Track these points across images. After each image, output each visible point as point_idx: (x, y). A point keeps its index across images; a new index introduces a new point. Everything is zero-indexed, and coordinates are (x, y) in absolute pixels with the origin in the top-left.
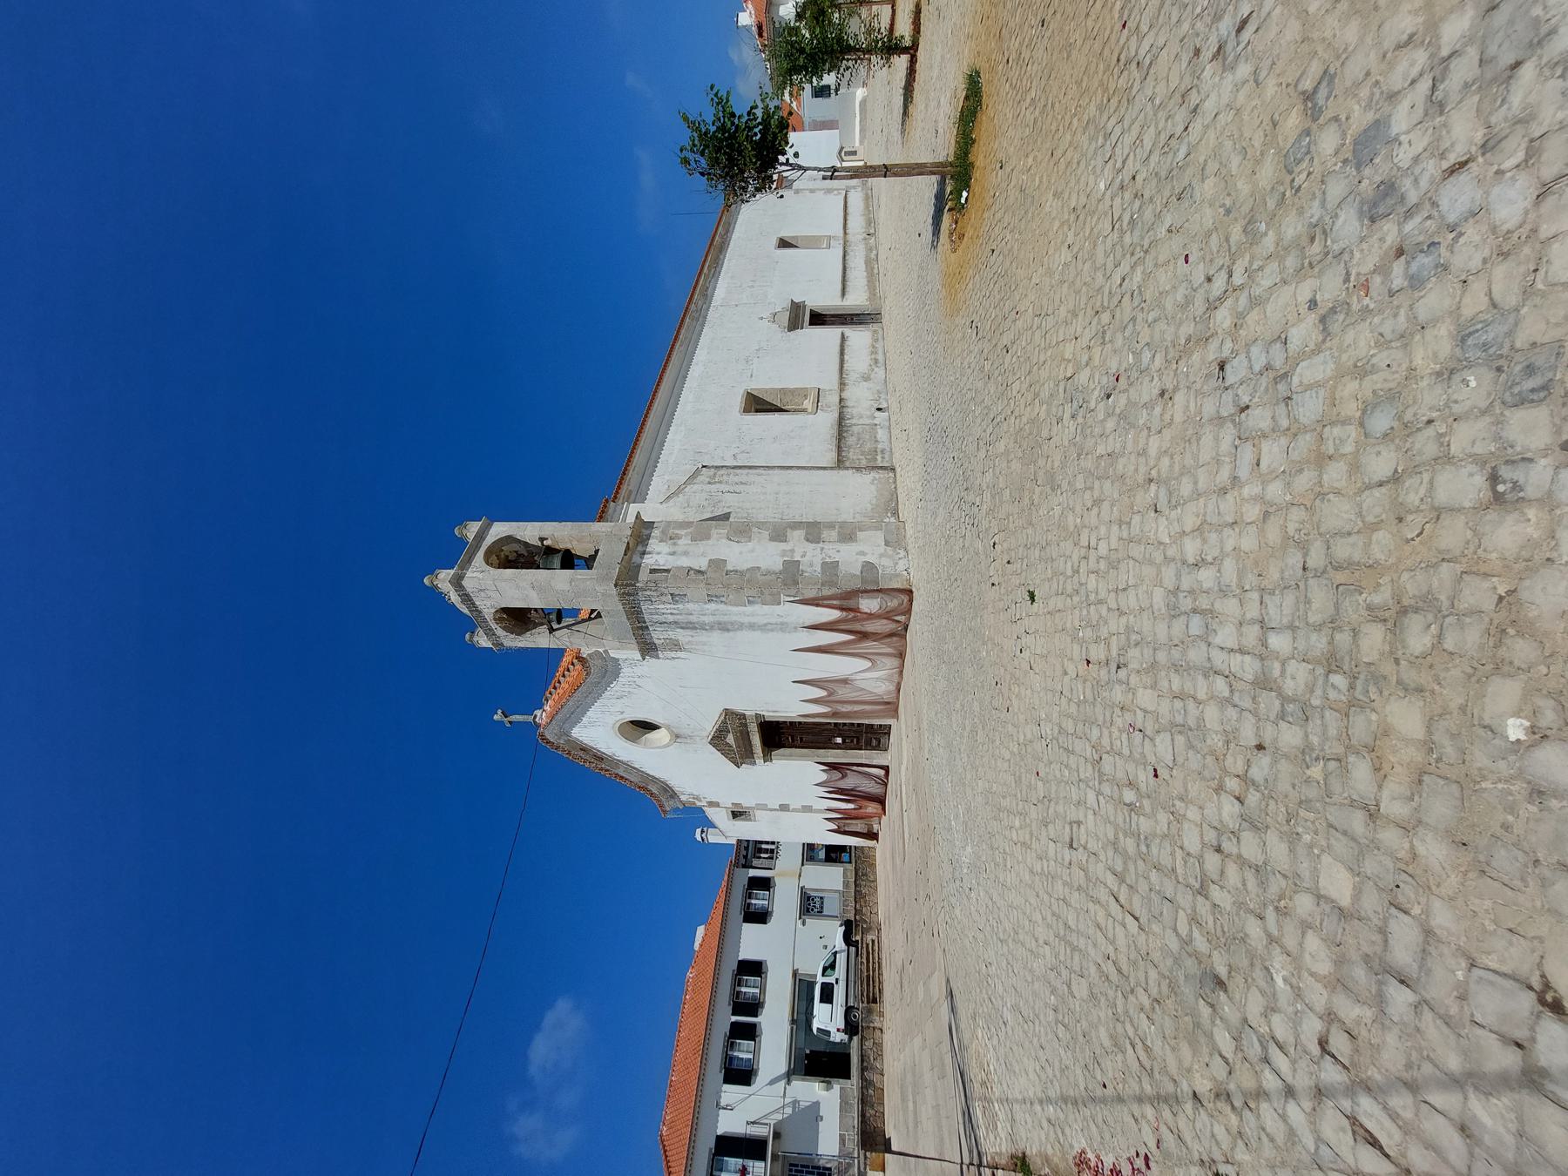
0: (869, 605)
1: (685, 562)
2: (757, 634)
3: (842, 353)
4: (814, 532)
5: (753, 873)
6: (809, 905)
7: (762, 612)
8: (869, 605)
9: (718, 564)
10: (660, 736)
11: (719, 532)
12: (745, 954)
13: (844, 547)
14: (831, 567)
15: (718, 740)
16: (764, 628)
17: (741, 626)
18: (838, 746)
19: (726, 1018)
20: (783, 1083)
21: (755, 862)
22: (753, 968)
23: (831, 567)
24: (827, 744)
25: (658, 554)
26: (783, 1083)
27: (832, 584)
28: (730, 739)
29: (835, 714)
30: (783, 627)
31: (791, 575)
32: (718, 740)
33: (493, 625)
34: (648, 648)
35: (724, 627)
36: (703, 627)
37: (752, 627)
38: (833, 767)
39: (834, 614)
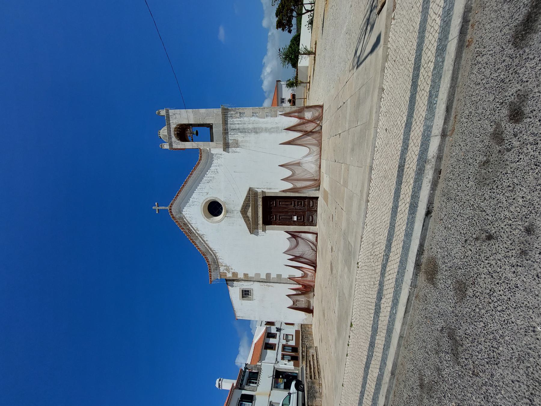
5: (244, 392)
21: (246, 387)
34: (226, 146)
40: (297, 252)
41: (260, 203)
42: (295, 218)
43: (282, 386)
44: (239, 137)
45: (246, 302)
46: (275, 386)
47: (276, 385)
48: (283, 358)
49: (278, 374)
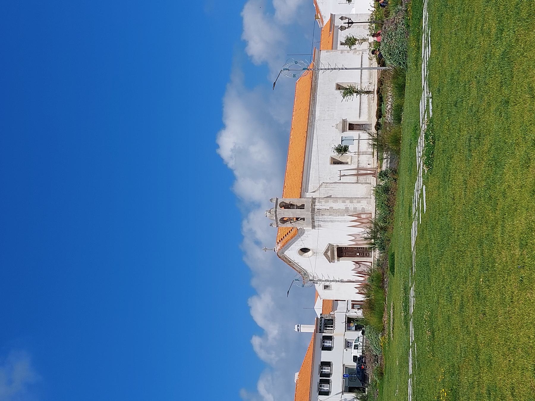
0: (363, 216)
1: (324, 207)
2: (339, 223)
3: (360, 109)
4: (351, 199)
5: (324, 334)
6: (348, 344)
7: (340, 218)
8: (363, 216)
9: (331, 208)
10: (310, 253)
11: (330, 200)
12: (323, 359)
13: (358, 204)
14: (355, 208)
15: (326, 254)
16: (340, 221)
17: (336, 221)
18: (358, 256)
19: (317, 378)
20: (341, 394)
21: (325, 331)
22: (328, 364)
23: (355, 208)
24: (354, 256)
25: (318, 206)
26: (341, 394)
27: (356, 212)
28: (329, 253)
29: (356, 244)
30: (345, 221)
31: (347, 210)
32: (326, 254)
33: (279, 221)
34: (314, 227)
35: (332, 221)
36: (327, 221)
37: (338, 221)
38: (357, 263)
39: (356, 218)
40: (360, 270)
41: (336, 250)
42: (358, 254)
43: (354, 328)
44: (321, 223)
45: (326, 291)
46: (348, 328)
47: (349, 328)
48: (353, 308)
49: (349, 320)
